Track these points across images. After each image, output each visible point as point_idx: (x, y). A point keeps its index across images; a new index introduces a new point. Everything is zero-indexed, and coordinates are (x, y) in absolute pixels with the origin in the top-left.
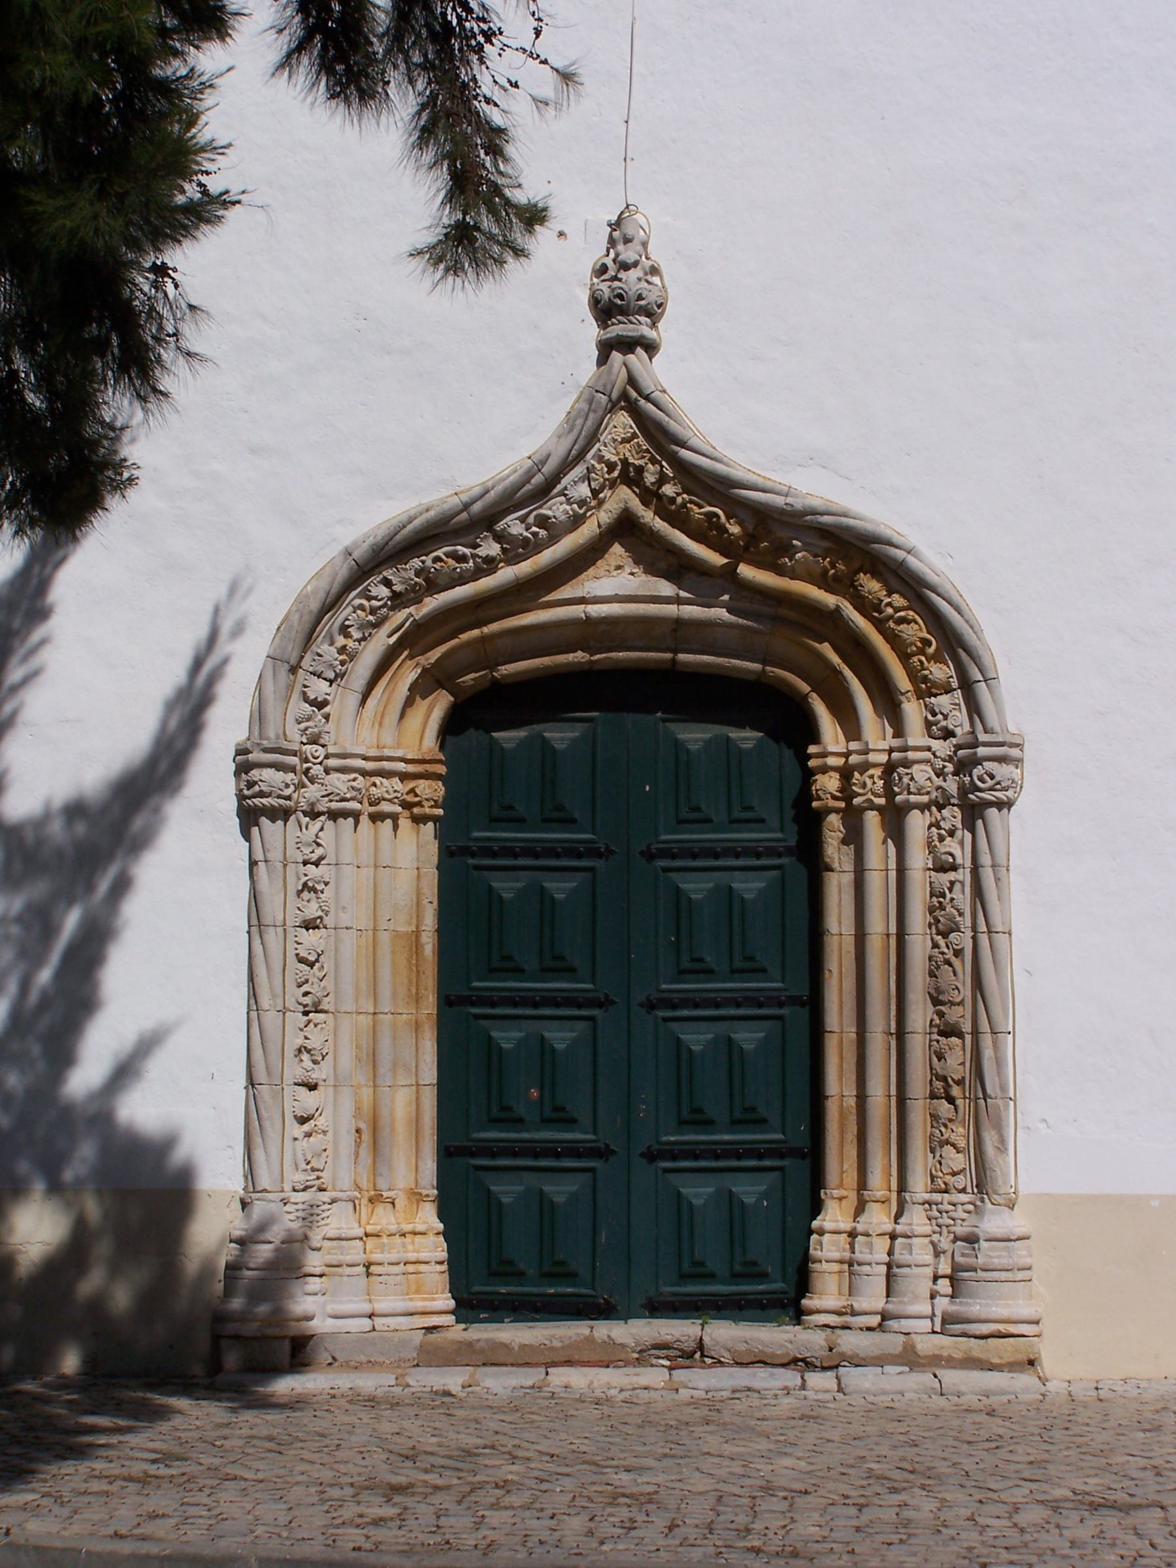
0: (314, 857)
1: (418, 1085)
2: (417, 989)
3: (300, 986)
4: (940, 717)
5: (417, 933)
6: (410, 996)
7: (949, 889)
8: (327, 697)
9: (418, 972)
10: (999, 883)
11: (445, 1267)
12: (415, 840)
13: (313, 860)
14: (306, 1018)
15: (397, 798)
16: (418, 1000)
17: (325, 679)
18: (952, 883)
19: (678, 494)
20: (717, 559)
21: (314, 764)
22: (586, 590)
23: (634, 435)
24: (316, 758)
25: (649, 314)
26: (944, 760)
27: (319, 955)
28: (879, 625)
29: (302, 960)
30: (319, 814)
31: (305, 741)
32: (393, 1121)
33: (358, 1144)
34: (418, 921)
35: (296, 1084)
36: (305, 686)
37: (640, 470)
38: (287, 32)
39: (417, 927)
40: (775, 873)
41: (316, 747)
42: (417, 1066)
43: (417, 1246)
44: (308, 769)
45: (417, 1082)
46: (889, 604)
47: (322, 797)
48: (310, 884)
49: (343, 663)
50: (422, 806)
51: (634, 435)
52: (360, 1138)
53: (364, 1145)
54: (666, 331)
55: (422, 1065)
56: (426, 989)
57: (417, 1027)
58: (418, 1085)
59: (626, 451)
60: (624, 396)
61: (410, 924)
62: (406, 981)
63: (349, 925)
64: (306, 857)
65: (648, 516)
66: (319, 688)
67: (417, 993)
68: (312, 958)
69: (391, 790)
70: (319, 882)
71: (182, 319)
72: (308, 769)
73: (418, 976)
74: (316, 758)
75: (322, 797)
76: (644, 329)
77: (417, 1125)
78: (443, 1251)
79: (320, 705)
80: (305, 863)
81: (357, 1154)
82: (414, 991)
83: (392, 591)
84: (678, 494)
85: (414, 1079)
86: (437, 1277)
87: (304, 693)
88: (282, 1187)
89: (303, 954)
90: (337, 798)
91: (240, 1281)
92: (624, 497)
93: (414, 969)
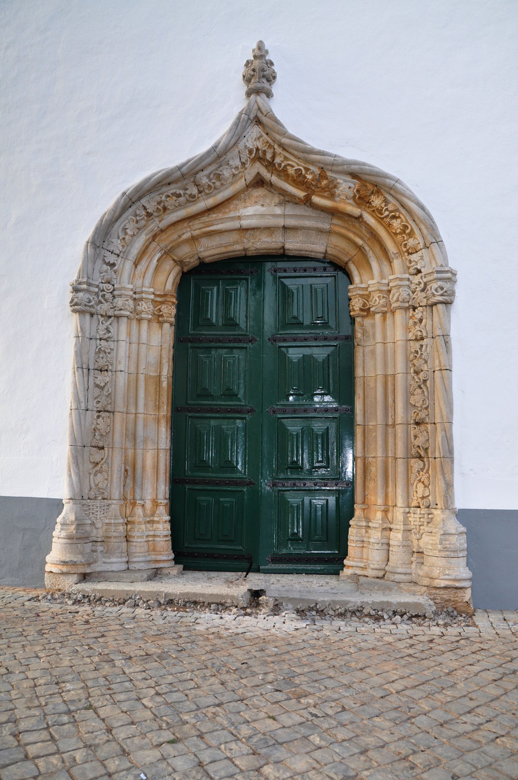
0: (106, 337)
1: (158, 449)
2: (159, 403)
3: (95, 399)
4: (413, 263)
5: (160, 376)
6: (155, 406)
7: (420, 349)
8: (115, 262)
9: (159, 395)
10: (448, 345)
11: (169, 538)
12: (160, 332)
13: (105, 338)
14: (98, 414)
15: (149, 311)
16: (158, 408)
17: (115, 254)
18: (422, 346)
19: (282, 162)
20: (301, 194)
21: (107, 293)
22: (240, 212)
23: (261, 136)
24: (108, 290)
25: (268, 81)
26: (417, 284)
27: (106, 384)
28: (380, 220)
29: (97, 386)
30: (110, 317)
31: (103, 282)
32: (143, 467)
33: (126, 477)
34: (160, 370)
35: (92, 446)
36: (104, 256)
37: (264, 152)
38: (238, 214)
39: (160, 373)
40: (334, 348)
41: (109, 285)
42: (158, 440)
43: (154, 528)
44: (104, 295)
45: (158, 447)
46: (387, 210)
47: (111, 308)
48: (103, 349)
49: (123, 246)
50: (163, 316)
51: (261, 136)
52: (127, 474)
53: (128, 477)
54: (276, 89)
55: (160, 439)
56: (163, 403)
57: (158, 421)
58: (158, 449)
59: (259, 144)
60: (256, 117)
61: (157, 372)
62: (154, 399)
63: (122, 369)
64: (101, 336)
65: (266, 175)
66: (112, 259)
67: (159, 405)
68: (102, 385)
69: (147, 308)
70: (107, 349)
71: (463, 599)
72: (104, 295)
73: (159, 397)
74: (109, 290)
75: (111, 308)
76: (266, 85)
77: (157, 469)
78: (168, 530)
79: (113, 265)
80: (101, 339)
81: (125, 481)
82: (157, 404)
83: (147, 212)
84: (282, 162)
85: (156, 445)
86: (162, 543)
87: (104, 260)
88: (418, 541)
89: (98, 382)
90: (118, 309)
91: (131, 543)
92: (259, 168)
93: (158, 393)
